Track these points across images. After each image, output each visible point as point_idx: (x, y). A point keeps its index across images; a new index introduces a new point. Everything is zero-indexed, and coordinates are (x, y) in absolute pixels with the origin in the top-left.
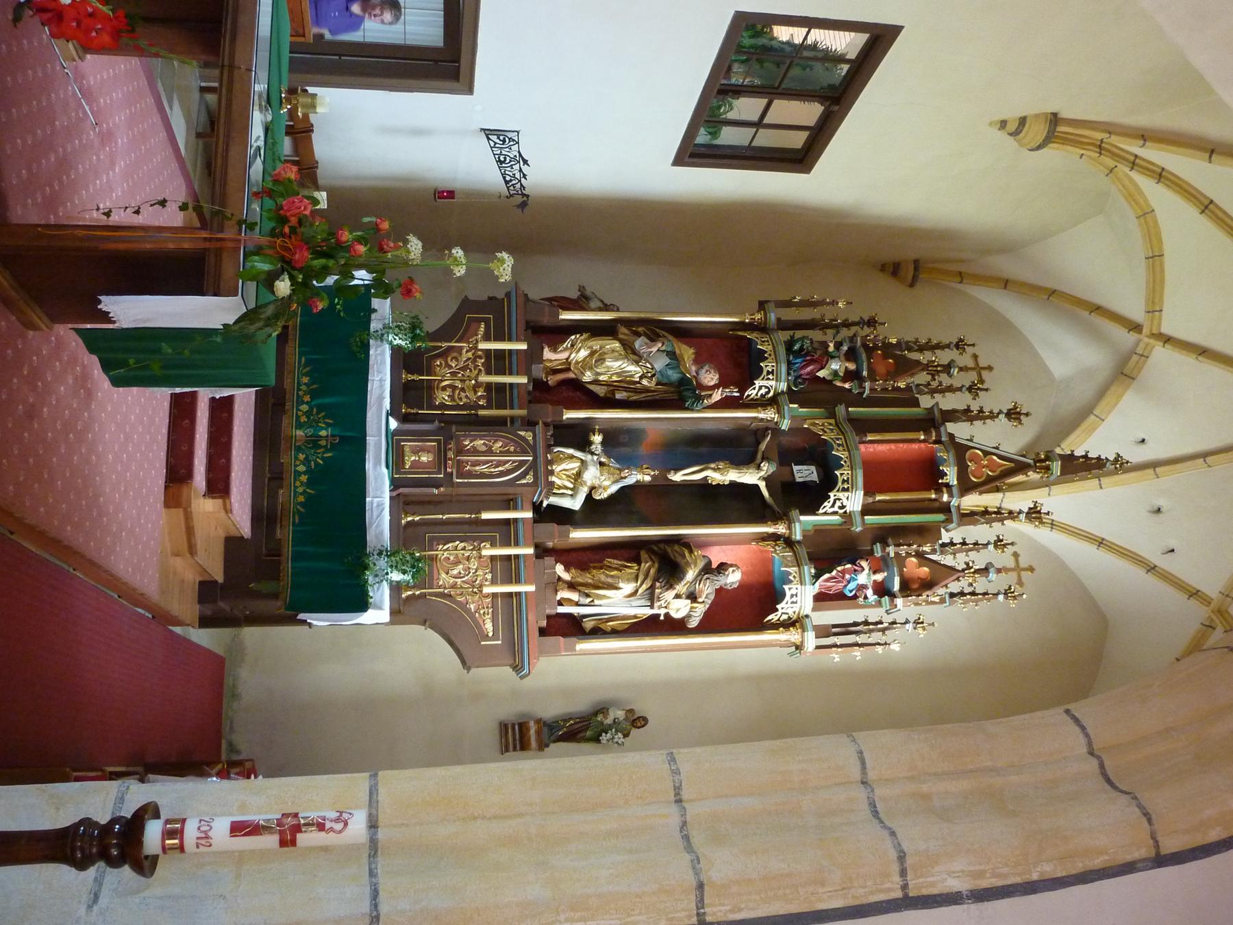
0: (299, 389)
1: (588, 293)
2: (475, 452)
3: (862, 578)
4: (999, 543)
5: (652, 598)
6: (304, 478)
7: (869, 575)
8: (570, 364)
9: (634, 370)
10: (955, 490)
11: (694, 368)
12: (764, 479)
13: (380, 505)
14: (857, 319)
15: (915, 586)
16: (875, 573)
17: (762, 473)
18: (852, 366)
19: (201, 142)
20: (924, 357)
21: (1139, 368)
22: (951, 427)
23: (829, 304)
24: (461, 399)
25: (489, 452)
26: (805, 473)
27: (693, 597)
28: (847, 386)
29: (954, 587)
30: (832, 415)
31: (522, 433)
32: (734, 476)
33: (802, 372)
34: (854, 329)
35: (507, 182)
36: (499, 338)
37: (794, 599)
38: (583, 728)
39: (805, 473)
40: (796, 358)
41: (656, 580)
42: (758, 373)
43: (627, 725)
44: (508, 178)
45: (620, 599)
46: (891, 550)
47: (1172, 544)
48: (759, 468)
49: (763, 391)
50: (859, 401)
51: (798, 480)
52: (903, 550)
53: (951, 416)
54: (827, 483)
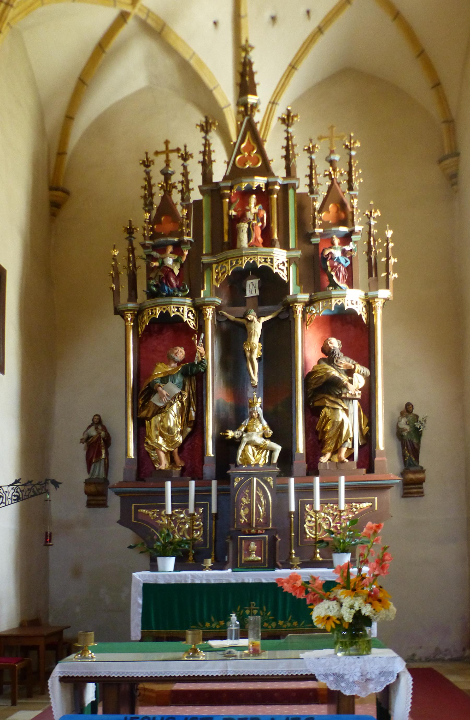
0: (215, 628)
1: (85, 437)
2: (249, 516)
3: (337, 253)
4: (310, 151)
5: (351, 399)
6: (295, 623)
7: (335, 249)
8: (168, 451)
9: (175, 408)
10: (272, 180)
11: (173, 365)
12: (259, 317)
13: (149, 576)
14: (127, 242)
15: (343, 215)
16: (333, 244)
17: (255, 319)
18: (170, 249)
19: (19, 701)
20: (157, 201)
21: (157, 19)
22: (218, 177)
23: (116, 263)
24: (199, 525)
25: (250, 506)
26: (252, 288)
27: (350, 372)
28: (186, 253)
29: (344, 183)
30: (209, 265)
31: (236, 484)
32: (255, 340)
33: (175, 285)
34: (136, 244)
35: (35, 495)
36: (163, 499)
37: (354, 302)
38: (409, 442)
39: (252, 288)
40: (164, 290)
41: (339, 396)
42: (178, 319)
43: (410, 417)
44: (32, 494)
45: (349, 419)
46: (318, 230)
47: (303, 11)
48: (251, 321)
49: (190, 315)
50: (197, 244)
51: (258, 293)
52: (318, 222)
53: (207, 175)
54: (266, 276)
